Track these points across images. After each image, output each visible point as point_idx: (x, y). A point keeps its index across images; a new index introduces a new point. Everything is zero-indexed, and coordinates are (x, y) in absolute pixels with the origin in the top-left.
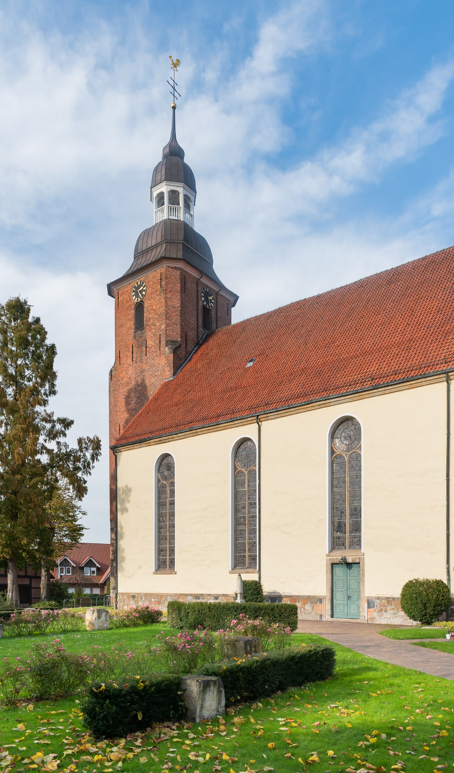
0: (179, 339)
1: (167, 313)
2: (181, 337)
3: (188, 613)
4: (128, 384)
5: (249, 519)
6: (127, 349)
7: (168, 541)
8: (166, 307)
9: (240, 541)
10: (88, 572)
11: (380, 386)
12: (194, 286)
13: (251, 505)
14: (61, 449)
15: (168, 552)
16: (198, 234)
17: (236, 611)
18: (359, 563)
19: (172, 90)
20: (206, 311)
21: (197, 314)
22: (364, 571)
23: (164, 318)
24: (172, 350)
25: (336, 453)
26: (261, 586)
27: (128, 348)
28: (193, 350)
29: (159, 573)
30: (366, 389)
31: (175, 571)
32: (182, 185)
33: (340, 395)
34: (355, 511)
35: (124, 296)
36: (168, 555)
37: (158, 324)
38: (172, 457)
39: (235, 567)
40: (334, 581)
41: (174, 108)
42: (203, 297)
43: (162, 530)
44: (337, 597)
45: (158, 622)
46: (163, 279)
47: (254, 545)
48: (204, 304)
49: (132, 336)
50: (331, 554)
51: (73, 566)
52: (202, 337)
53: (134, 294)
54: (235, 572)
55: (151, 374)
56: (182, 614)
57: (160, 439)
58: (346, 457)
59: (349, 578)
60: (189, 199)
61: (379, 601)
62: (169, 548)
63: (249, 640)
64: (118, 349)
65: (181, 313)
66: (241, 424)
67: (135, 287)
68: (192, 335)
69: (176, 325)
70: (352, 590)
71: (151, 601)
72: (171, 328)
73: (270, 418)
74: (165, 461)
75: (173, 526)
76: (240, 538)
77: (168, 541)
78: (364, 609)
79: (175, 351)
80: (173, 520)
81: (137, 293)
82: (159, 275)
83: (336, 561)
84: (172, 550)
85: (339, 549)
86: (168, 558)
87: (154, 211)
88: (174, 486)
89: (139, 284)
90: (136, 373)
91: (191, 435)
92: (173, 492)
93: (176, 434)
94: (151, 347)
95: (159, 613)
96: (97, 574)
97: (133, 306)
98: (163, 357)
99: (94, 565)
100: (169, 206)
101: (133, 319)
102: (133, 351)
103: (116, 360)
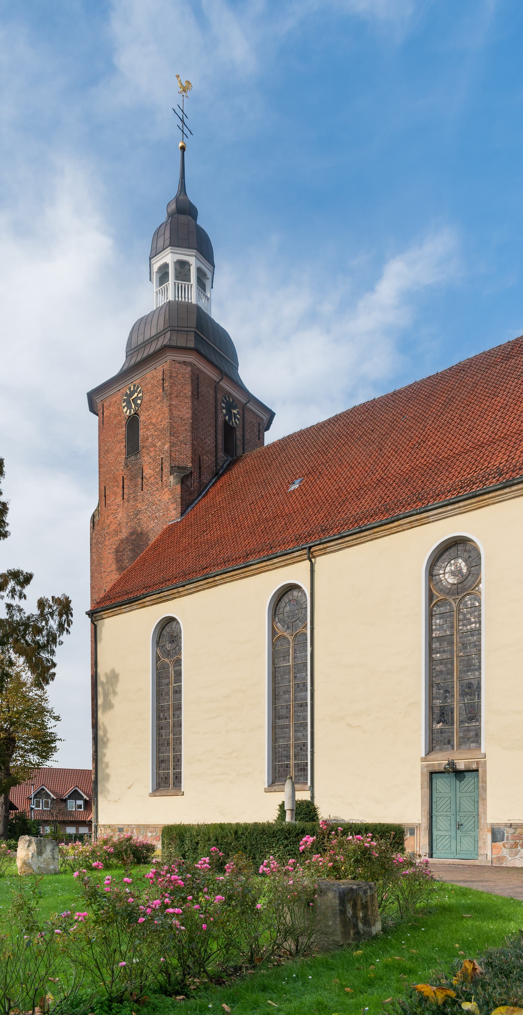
0: (190, 465)
1: (172, 427)
2: (193, 461)
3: (197, 843)
4: (117, 532)
5: (296, 709)
6: (115, 484)
7: (171, 747)
8: (171, 419)
9: (281, 742)
10: (72, 805)
11: (515, 482)
12: (212, 392)
13: (298, 687)
14: (13, 615)
15: (171, 763)
16: (218, 326)
17: (286, 838)
18: (477, 771)
19: (180, 124)
20: (229, 430)
21: (216, 431)
22: (486, 783)
23: (168, 435)
24: (179, 479)
25: (437, 597)
26: (315, 809)
27: (117, 481)
28: (210, 482)
29: (158, 794)
30: (490, 489)
31: (182, 790)
32: (194, 254)
33: (446, 503)
34: (469, 688)
35: (111, 409)
36: (171, 767)
37: (159, 444)
38: (178, 622)
39: (273, 783)
40: (434, 800)
41: (183, 149)
42: (224, 408)
43: (163, 732)
44: (438, 826)
45: (148, 863)
46: (167, 378)
47: (304, 748)
48: (225, 419)
49: (123, 464)
50: (430, 757)
51: (53, 798)
52: (223, 465)
53: (125, 404)
54: (273, 790)
55: (149, 517)
56: (186, 846)
57: (159, 596)
58: (453, 603)
59: (459, 795)
60: (205, 275)
61: (511, 831)
62: (174, 757)
63: (352, 889)
64: (103, 485)
65: (192, 427)
66: (283, 564)
67: (126, 395)
68: (208, 460)
69: (186, 444)
70: (464, 814)
71: (146, 835)
72: (177, 448)
73: (329, 550)
74: (168, 629)
75: (179, 725)
76: (282, 738)
77: (171, 747)
78: (485, 843)
79: (183, 481)
80: (180, 716)
81: (130, 402)
82: (161, 373)
83: (437, 769)
84: (178, 761)
85: (441, 750)
86: (171, 771)
87: (155, 291)
88: (181, 665)
89: (132, 389)
90: (128, 516)
91: (206, 586)
92: (178, 674)
93: (184, 586)
94: (150, 478)
95: (150, 848)
96: (85, 808)
97: (124, 422)
98: (166, 489)
99: (81, 798)
100: (175, 283)
101: (124, 440)
102: (123, 486)
103: (99, 500)
